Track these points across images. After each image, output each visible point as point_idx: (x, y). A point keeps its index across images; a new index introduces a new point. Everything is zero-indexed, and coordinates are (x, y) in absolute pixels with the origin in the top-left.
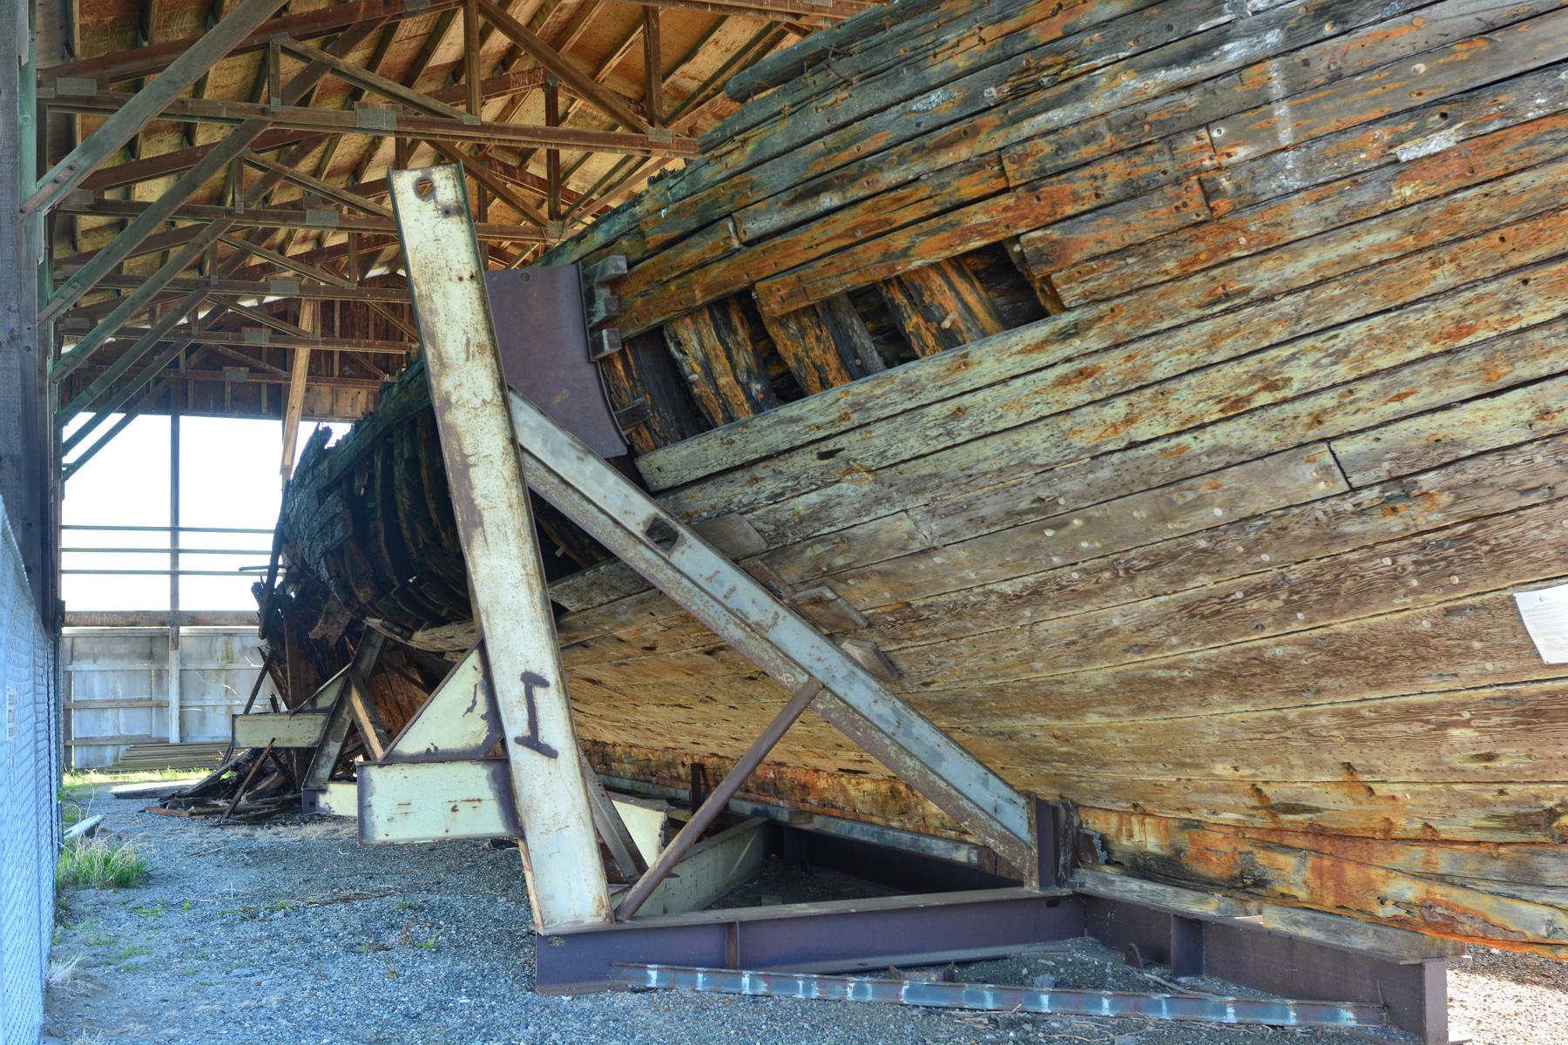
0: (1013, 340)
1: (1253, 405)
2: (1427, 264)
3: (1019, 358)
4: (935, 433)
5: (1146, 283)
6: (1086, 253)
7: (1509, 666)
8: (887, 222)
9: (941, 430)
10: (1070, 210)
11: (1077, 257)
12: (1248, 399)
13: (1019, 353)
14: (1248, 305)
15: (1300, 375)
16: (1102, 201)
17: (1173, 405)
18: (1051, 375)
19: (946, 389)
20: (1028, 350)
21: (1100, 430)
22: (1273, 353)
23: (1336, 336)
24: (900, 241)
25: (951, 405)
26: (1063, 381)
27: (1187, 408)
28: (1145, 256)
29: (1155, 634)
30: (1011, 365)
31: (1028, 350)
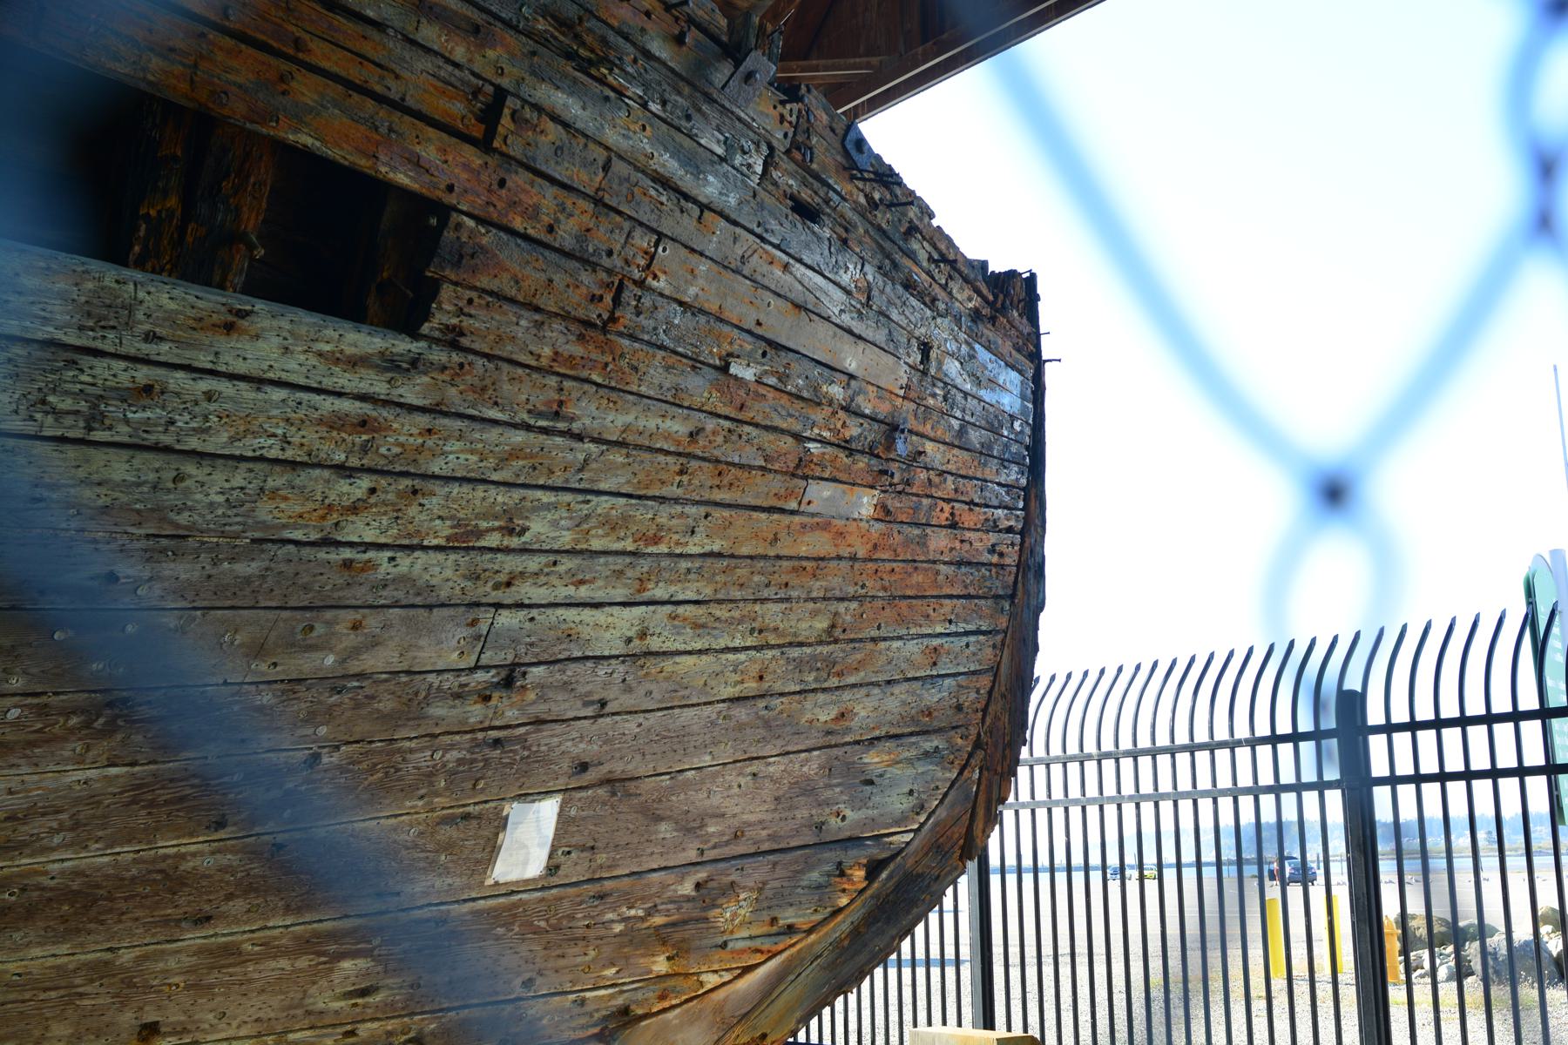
0: (329, 333)
1: (482, 543)
2: (677, 468)
3: (313, 361)
4: (67, 404)
5: (515, 357)
6: (494, 285)
7: (458, 882)
8: (297, 43)
9: (83, 406)
10: (518, 223)
11: (484, 281)
12: (480, 534)
13: (320, 354)
14: (562, 433)
15: (538, 527)
16: (547, 238)
17: (413, 511)
18: (328, 404)
19: (165, 347)
20: (335, 359)
21: (310, 506)
22: (539, 494)
23: (588, 502)
24: (306, 89)
25: (143, 374)
26: (335, 423)
27: (836, 582)
28: (539, 325)
29: (38, 826)
30: (295, 367)
31: (335, 359)
